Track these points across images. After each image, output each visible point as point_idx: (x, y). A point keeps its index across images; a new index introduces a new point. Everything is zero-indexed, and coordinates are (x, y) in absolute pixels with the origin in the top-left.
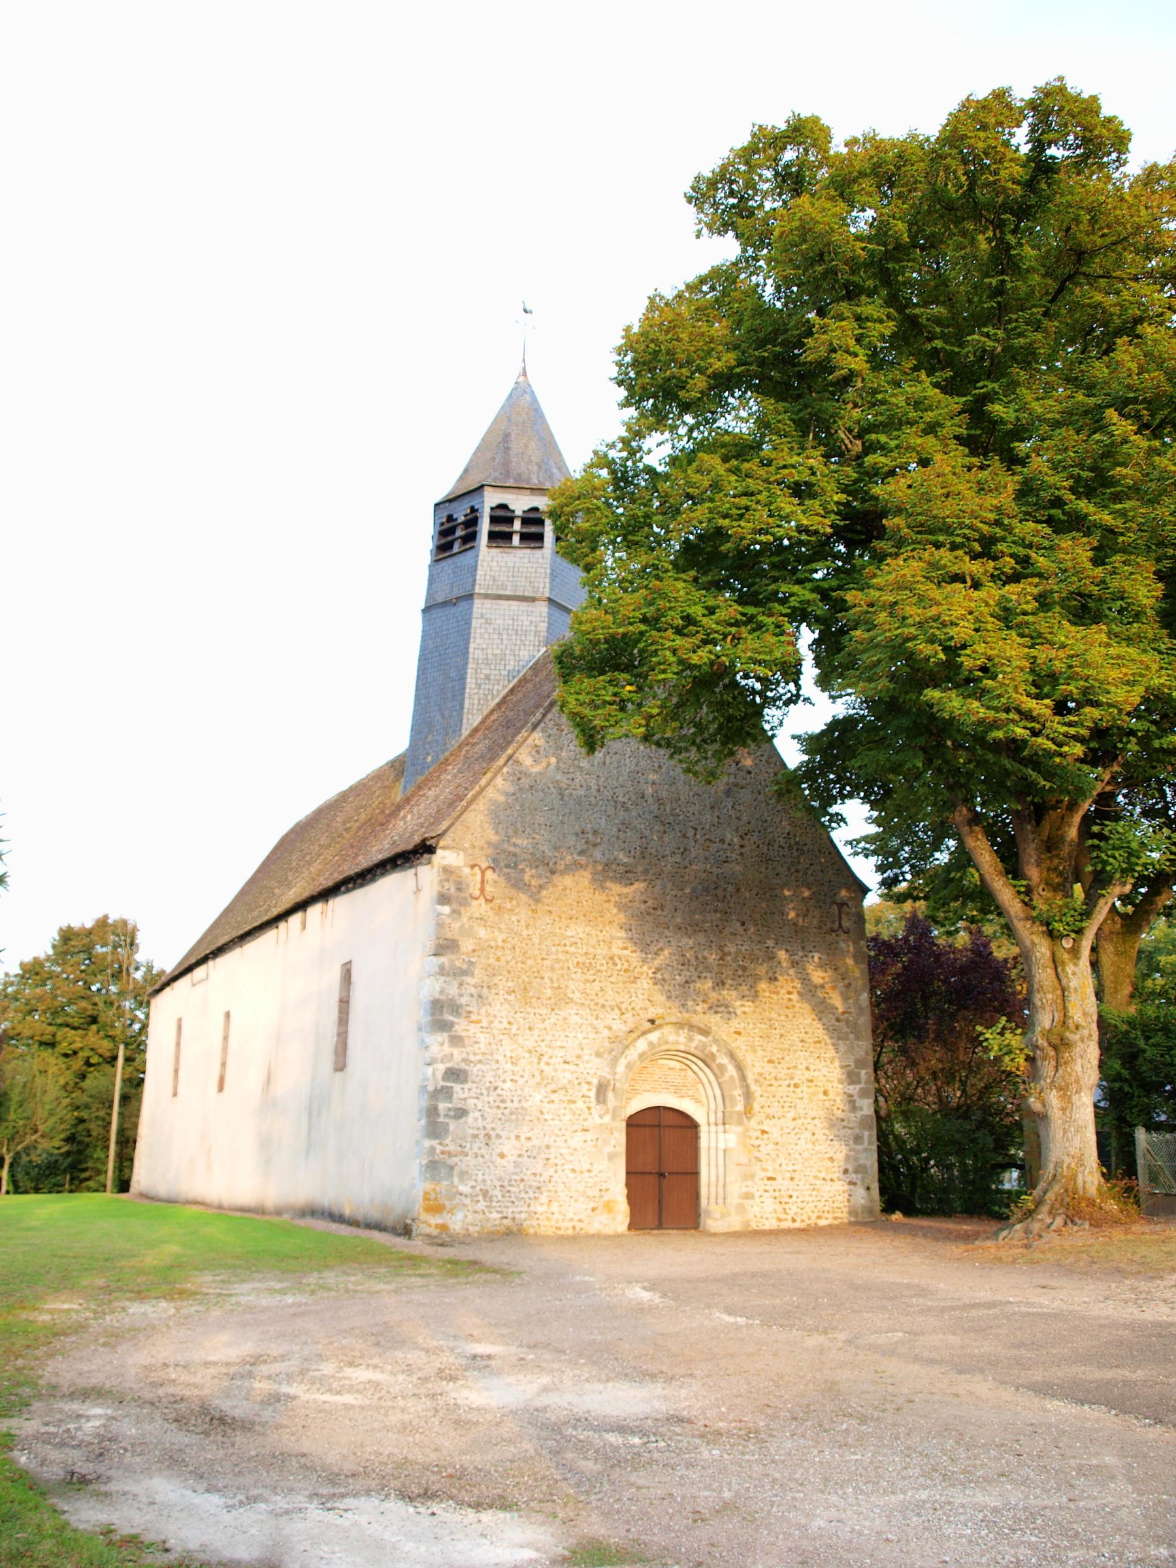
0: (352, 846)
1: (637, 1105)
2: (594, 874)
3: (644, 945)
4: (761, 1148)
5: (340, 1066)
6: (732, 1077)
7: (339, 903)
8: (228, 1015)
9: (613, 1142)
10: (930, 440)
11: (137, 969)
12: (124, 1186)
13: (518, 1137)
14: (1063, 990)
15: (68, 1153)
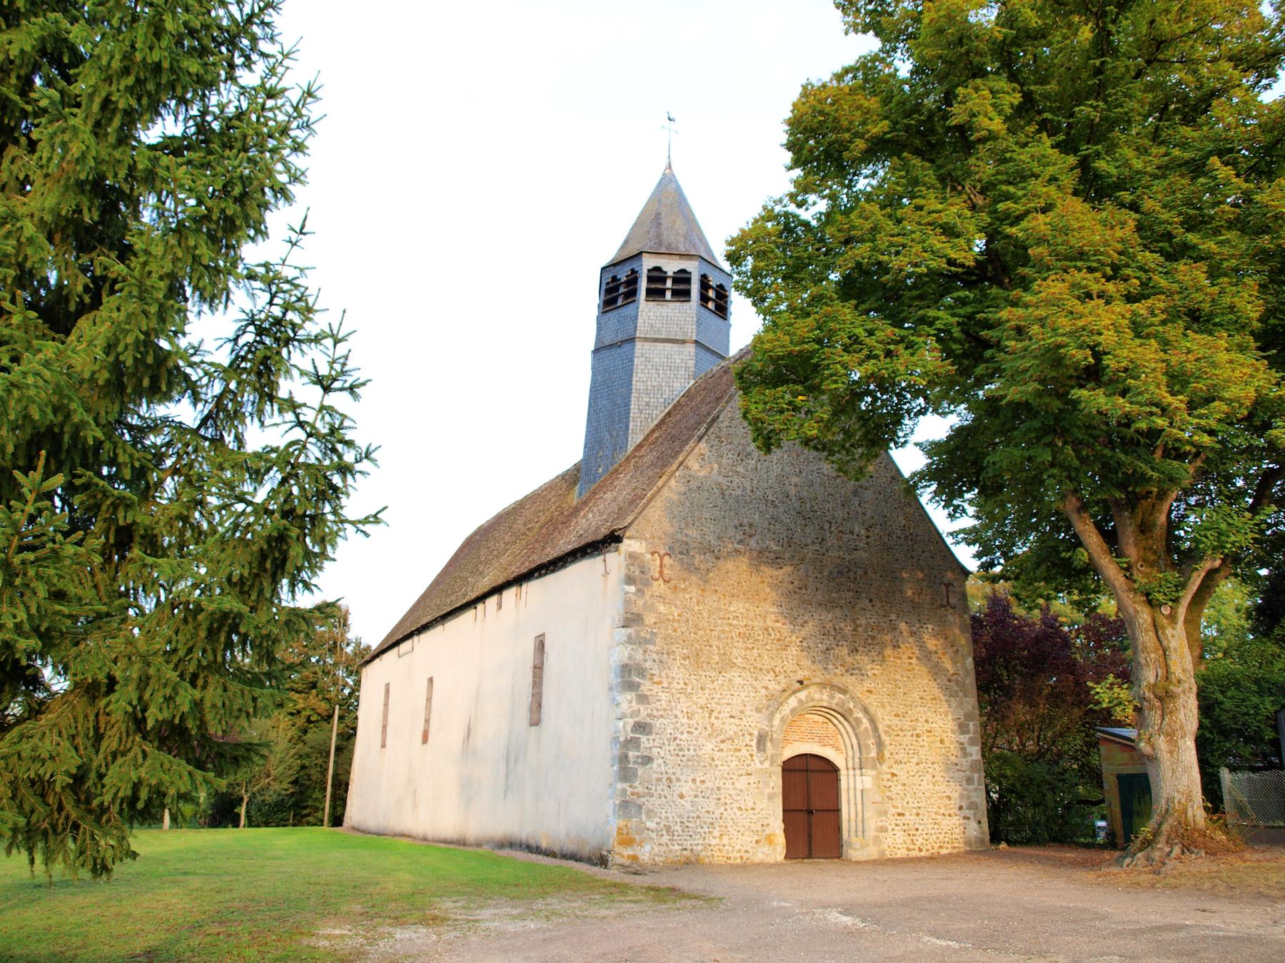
0: (537, 541)
1: (789, 753)
2: (750, 559)
3: (793, 620)
5: (535, 721)
7: (533, 588)
8: (431, 680)
10: (1052, 188)
11: (348, 645)
12: (337, 821)
13: (694, 780)
14: (1164, 651)
15: (292, 794)
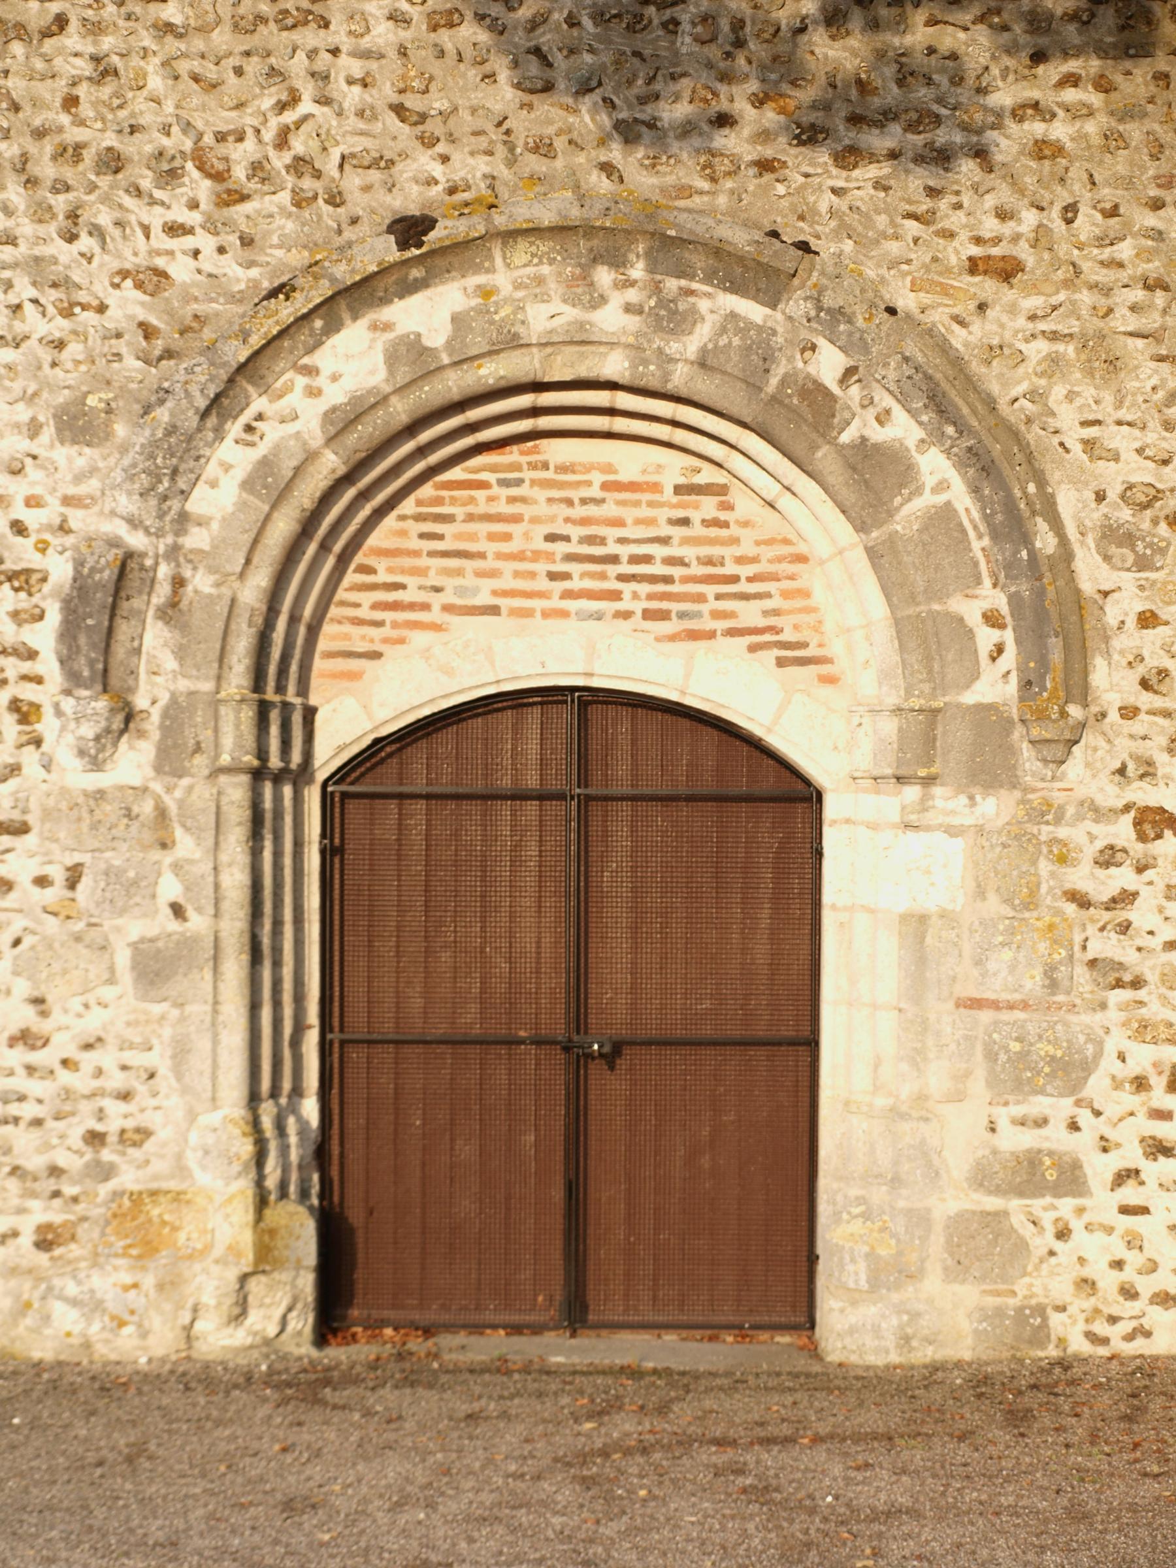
4: (1141, 915)
6: (947, 512)
9: (170, 888)
